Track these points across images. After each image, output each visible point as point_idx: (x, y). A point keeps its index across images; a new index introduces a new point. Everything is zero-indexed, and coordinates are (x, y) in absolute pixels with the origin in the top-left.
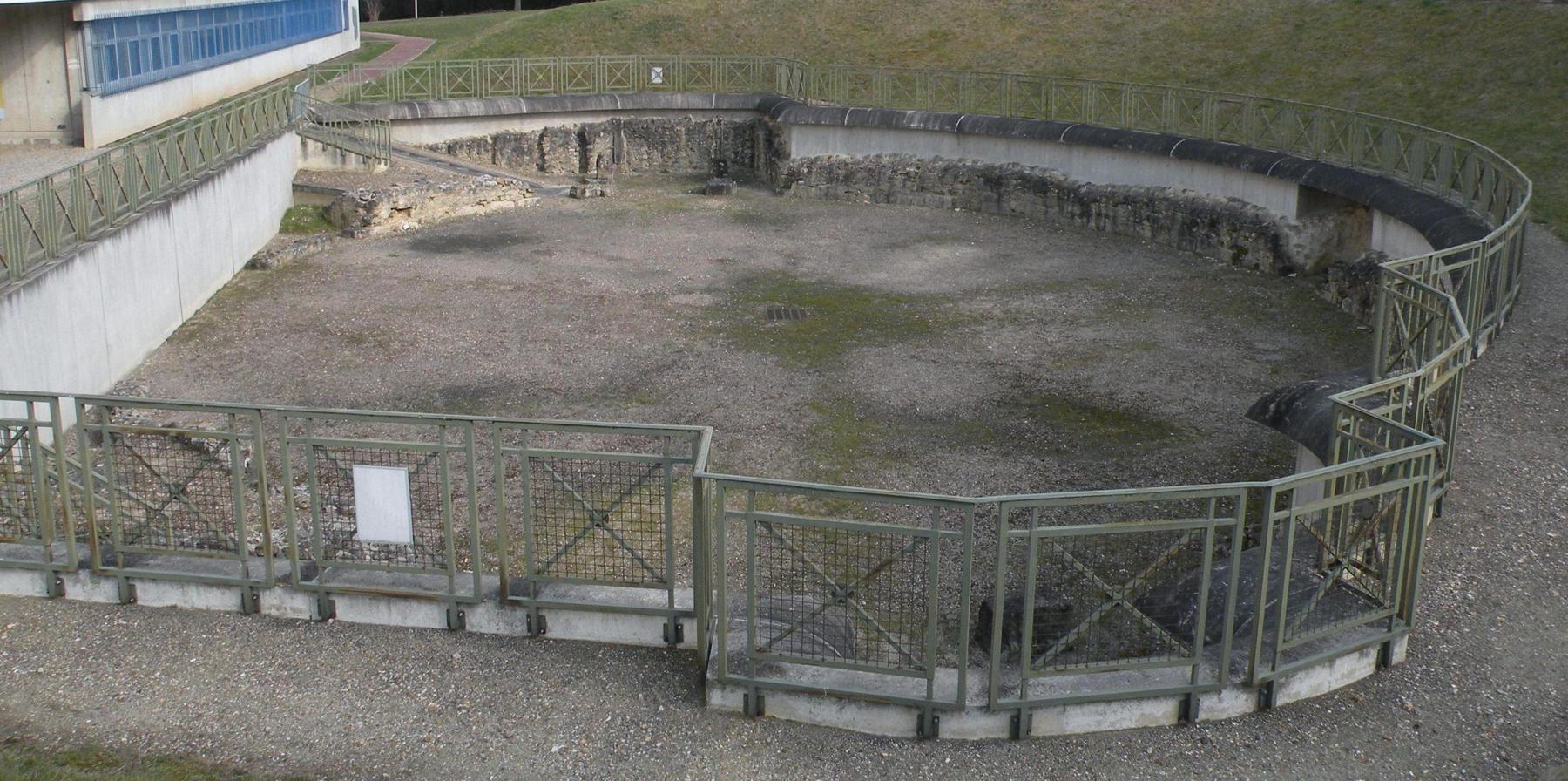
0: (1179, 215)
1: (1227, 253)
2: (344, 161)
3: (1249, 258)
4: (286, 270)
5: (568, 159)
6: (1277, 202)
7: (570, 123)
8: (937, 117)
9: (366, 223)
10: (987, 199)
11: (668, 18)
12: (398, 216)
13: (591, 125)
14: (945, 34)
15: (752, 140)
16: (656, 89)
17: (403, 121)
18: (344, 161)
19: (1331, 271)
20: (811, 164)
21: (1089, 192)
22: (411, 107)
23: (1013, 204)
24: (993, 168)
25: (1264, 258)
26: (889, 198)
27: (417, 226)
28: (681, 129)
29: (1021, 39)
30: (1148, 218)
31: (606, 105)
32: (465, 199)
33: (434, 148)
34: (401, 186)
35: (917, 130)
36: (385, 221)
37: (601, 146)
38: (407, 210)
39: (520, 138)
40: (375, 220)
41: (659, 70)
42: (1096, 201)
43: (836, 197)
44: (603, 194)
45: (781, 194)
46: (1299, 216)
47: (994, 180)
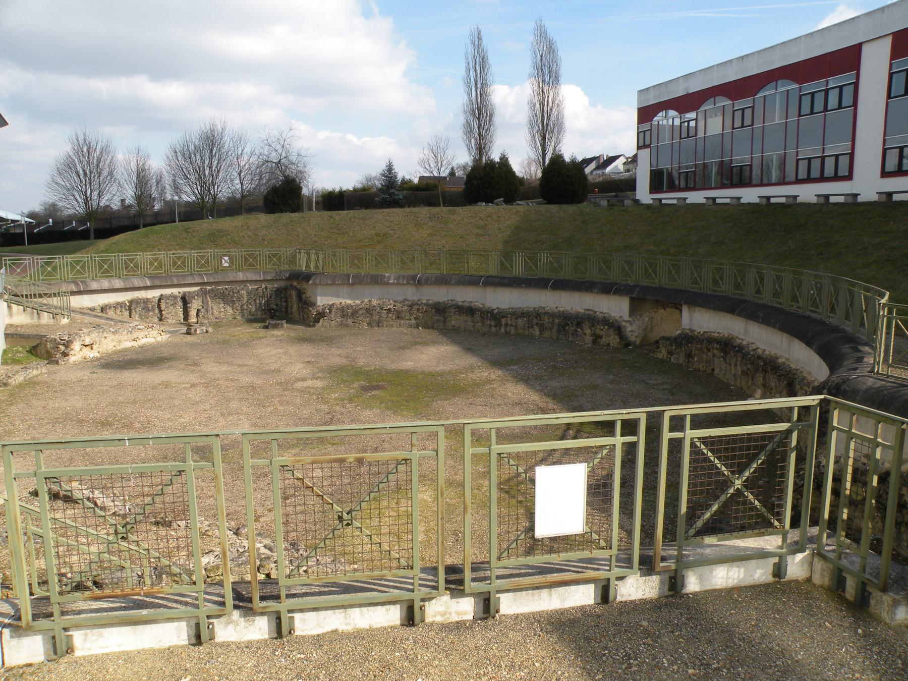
0: (557, 321)
1: (589, 339)
2: (39, 317)
3: (603, 341)
4: (21, 386)
5: (176, 312)
6: (616, 307)
7: (175, 291)
8: (404, 277)
9: (65, 354)
10: (437, 321)
11: (220, 231)
12: (85, 349)
13: (189, 292)
14: (385, 234)
15: (286, 297)
16: (225, 270)
17: (73, 293)
18: (39, 317)
19: (661, 342)
20: (331, 307)
21: (499, 313)
22: (76, 283)
23: (453, 323)
24: (439, 303)
25: (614, 340)
26: (379, 324)
27: (98, 355)
28: (244, 292)
29: (431, 235)
30: (537, 324)
31: (198, 280)
32: (126, 337)
33: (93, 309)
34: (86, 331)
35: (393, 284)
36: (77, 353)
37: (195, 305)
38: (91, 346)
39: (146, 301)
40: (72, 352)
41: (227, 258)
42: (504, 317)
43: (347, 326)
44: (207, 332)
45: (314, 326)
46: (630, 315)
47: (440, 309)
